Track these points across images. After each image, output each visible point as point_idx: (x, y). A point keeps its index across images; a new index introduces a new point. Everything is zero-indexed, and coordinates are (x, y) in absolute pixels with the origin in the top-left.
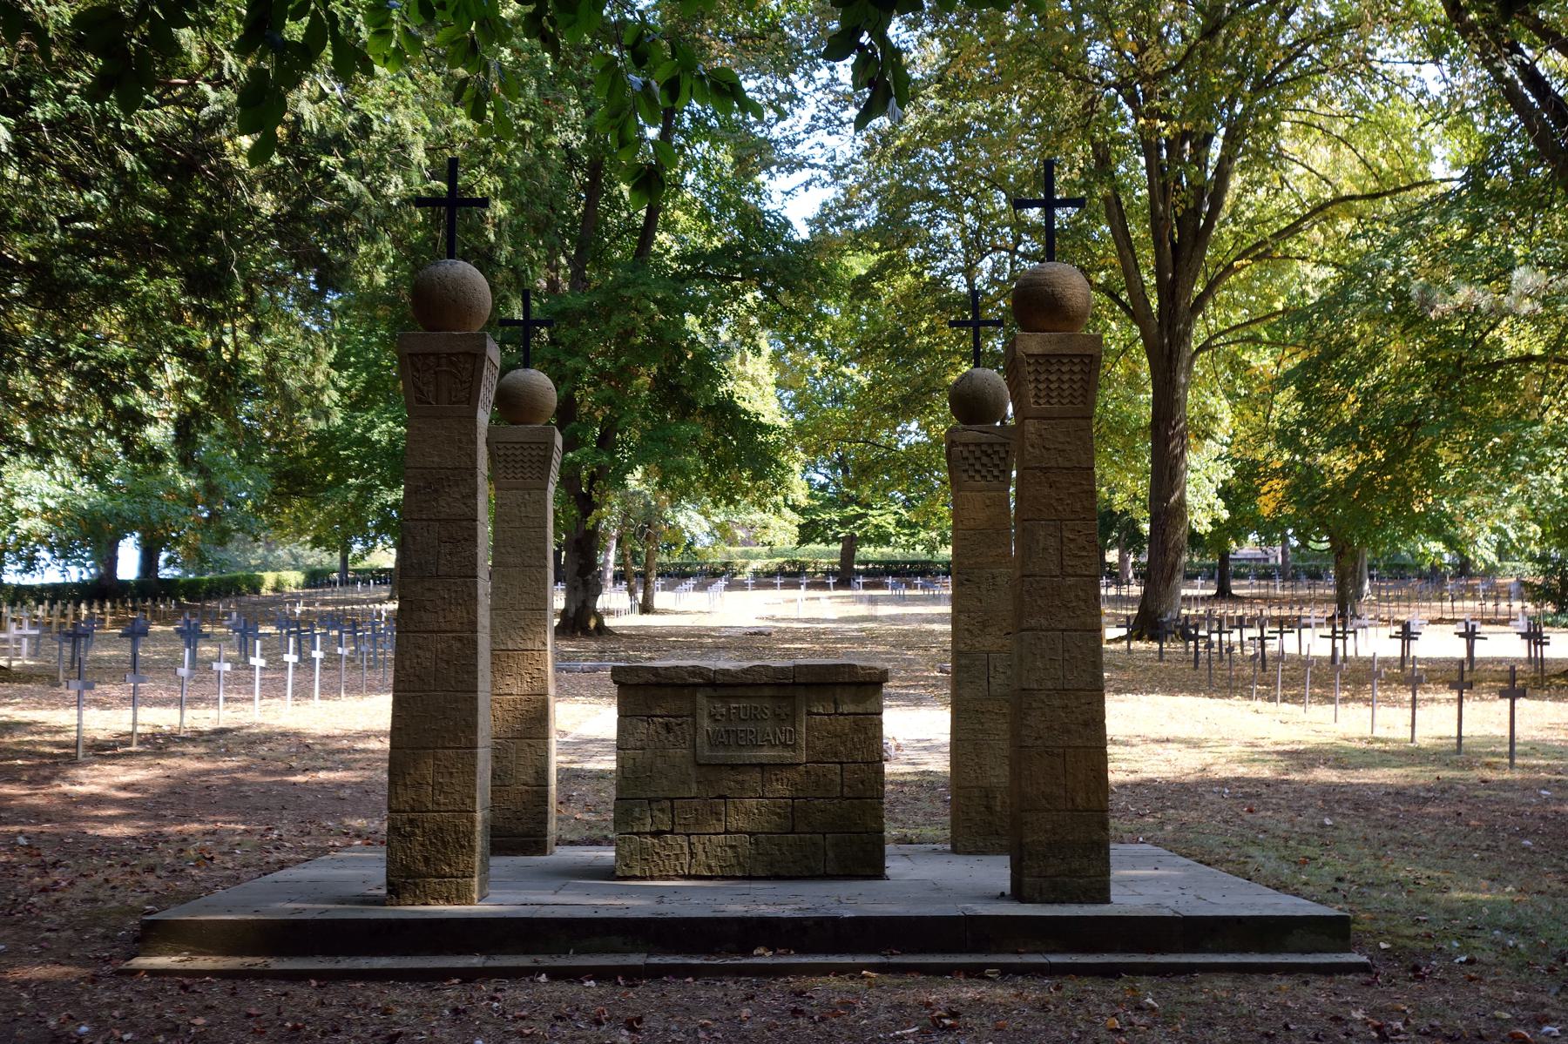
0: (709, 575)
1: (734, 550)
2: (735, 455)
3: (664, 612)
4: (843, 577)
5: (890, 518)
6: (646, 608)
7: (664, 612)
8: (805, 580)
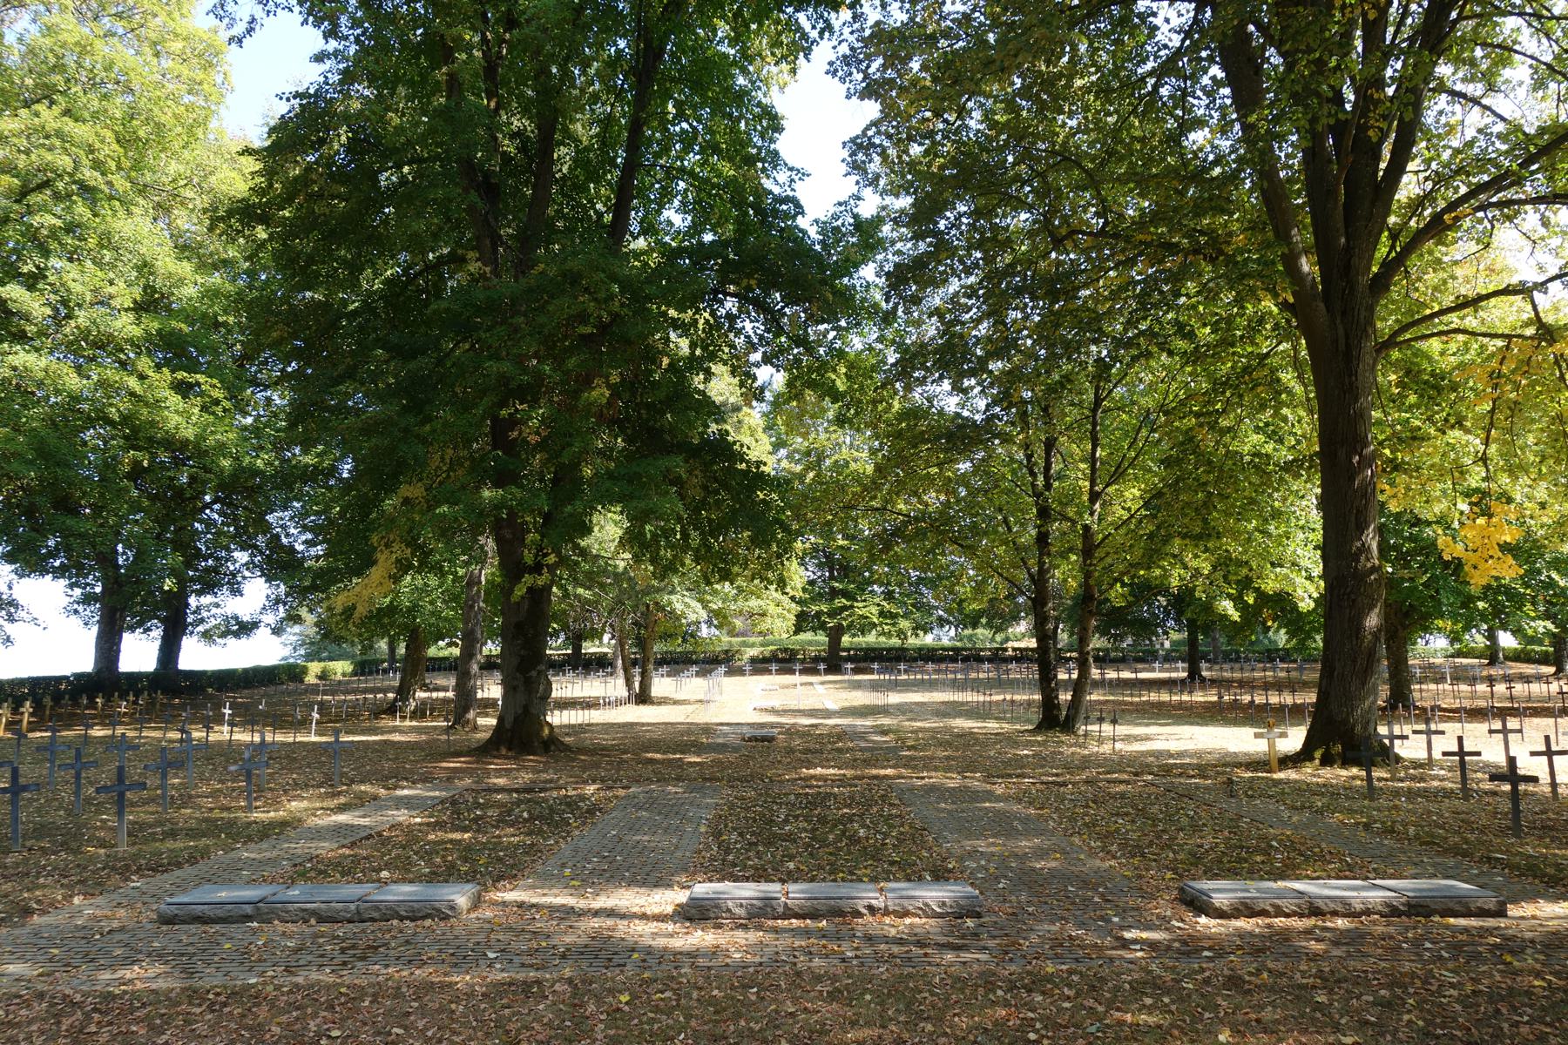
1: (734, 640)
2: (727, 513)
3: (663, 701)
4: (832, 661)
5: (875, 610)
6: (643, 698)
7: (663, 701)
8: (798, 667)
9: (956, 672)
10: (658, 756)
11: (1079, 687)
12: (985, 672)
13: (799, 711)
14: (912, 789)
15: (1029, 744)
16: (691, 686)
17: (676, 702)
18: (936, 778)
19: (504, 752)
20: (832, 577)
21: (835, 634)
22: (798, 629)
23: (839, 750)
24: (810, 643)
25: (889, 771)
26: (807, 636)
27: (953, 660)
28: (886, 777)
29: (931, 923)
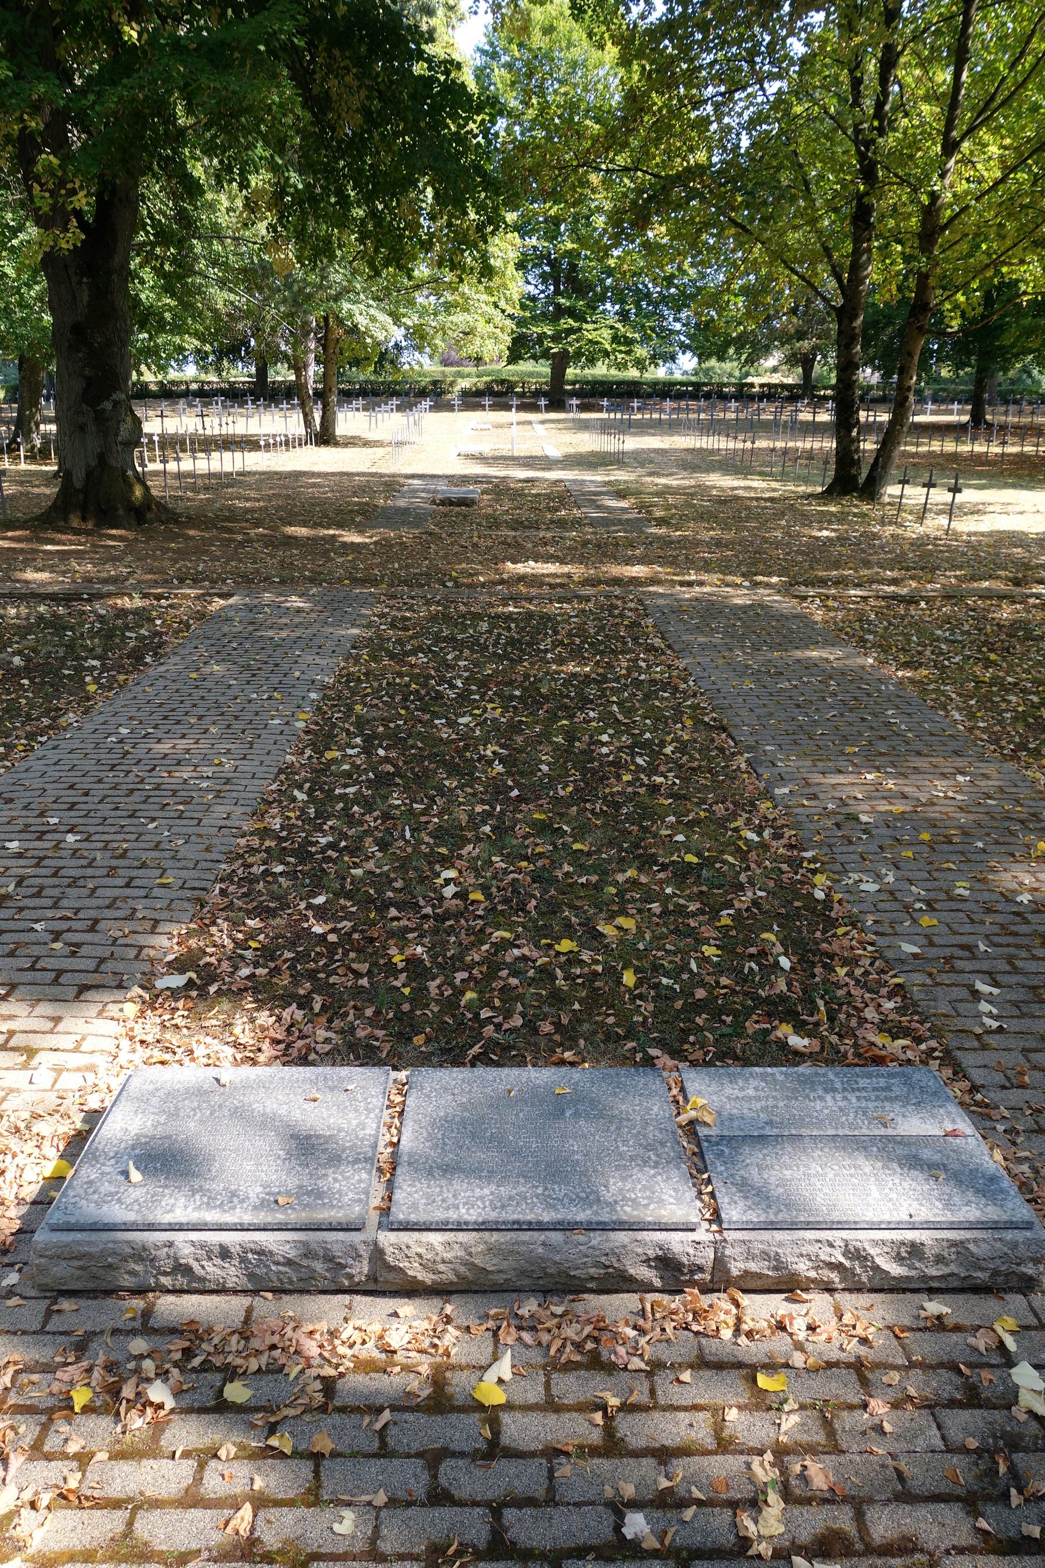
0: (411, 394)
1: (449, 370)
3: (351, 442)
4: (554, 397)
5: (607, 334)
6: (325, 437)
7: (351, 442)
9: (697, 412)
10: (302, 531)
11: (890, 437)
12: (731, 413)
13: (513, 458)
14: (678, 609)
15: (825, 520)
16: (387, 423)
17: (367, 444)
18: (710, 586)
19: (75, 523)
20: (557, 292)
21: (560, 362)
22: (514, 357)
23: (562, 523)
24: (531, 374)
25: (638, 571)
26: (526, 366)
27: (694, 396)
28: (635, 581)
29: (870, 1317)
